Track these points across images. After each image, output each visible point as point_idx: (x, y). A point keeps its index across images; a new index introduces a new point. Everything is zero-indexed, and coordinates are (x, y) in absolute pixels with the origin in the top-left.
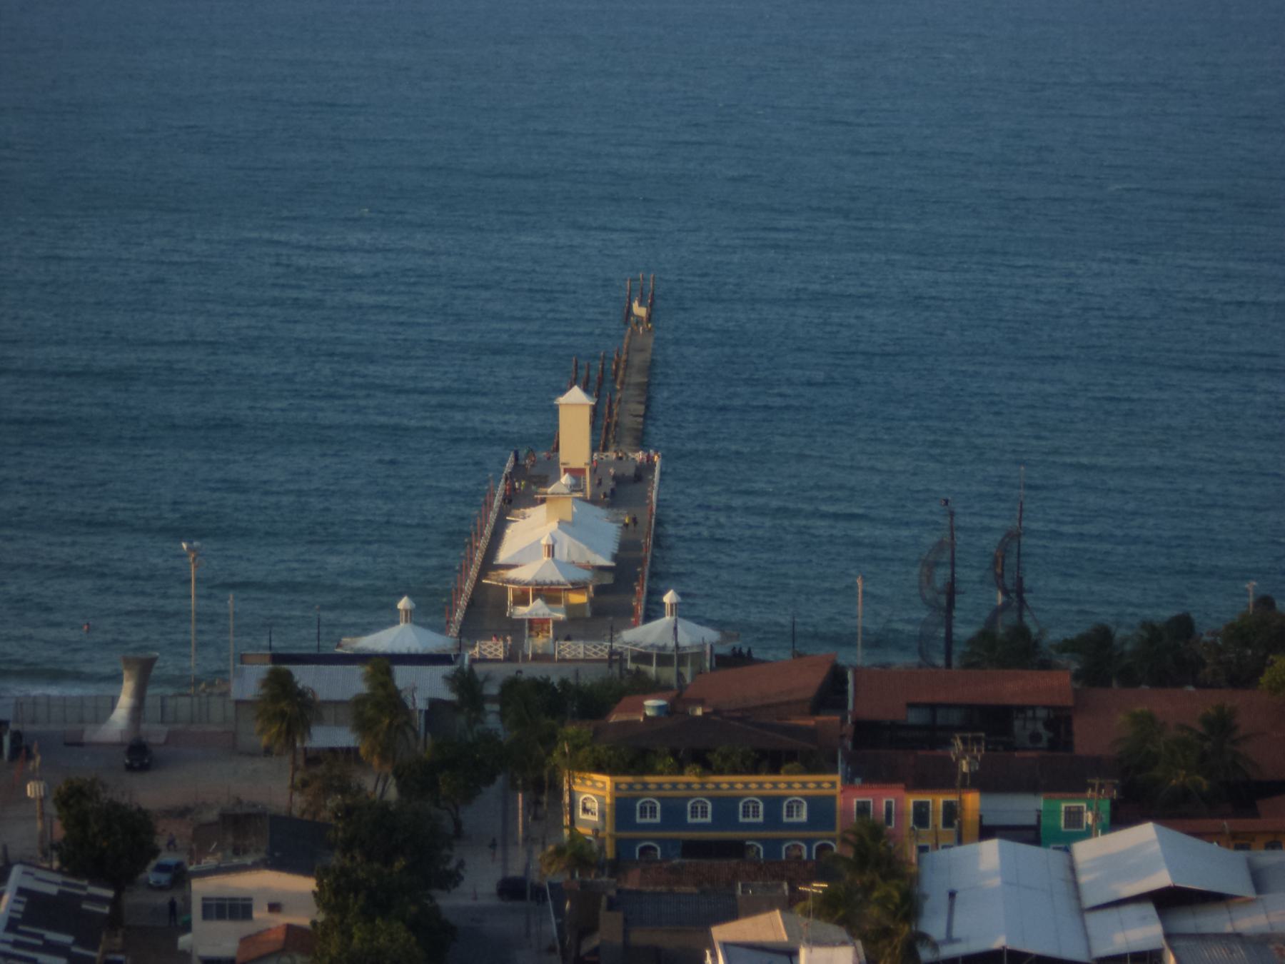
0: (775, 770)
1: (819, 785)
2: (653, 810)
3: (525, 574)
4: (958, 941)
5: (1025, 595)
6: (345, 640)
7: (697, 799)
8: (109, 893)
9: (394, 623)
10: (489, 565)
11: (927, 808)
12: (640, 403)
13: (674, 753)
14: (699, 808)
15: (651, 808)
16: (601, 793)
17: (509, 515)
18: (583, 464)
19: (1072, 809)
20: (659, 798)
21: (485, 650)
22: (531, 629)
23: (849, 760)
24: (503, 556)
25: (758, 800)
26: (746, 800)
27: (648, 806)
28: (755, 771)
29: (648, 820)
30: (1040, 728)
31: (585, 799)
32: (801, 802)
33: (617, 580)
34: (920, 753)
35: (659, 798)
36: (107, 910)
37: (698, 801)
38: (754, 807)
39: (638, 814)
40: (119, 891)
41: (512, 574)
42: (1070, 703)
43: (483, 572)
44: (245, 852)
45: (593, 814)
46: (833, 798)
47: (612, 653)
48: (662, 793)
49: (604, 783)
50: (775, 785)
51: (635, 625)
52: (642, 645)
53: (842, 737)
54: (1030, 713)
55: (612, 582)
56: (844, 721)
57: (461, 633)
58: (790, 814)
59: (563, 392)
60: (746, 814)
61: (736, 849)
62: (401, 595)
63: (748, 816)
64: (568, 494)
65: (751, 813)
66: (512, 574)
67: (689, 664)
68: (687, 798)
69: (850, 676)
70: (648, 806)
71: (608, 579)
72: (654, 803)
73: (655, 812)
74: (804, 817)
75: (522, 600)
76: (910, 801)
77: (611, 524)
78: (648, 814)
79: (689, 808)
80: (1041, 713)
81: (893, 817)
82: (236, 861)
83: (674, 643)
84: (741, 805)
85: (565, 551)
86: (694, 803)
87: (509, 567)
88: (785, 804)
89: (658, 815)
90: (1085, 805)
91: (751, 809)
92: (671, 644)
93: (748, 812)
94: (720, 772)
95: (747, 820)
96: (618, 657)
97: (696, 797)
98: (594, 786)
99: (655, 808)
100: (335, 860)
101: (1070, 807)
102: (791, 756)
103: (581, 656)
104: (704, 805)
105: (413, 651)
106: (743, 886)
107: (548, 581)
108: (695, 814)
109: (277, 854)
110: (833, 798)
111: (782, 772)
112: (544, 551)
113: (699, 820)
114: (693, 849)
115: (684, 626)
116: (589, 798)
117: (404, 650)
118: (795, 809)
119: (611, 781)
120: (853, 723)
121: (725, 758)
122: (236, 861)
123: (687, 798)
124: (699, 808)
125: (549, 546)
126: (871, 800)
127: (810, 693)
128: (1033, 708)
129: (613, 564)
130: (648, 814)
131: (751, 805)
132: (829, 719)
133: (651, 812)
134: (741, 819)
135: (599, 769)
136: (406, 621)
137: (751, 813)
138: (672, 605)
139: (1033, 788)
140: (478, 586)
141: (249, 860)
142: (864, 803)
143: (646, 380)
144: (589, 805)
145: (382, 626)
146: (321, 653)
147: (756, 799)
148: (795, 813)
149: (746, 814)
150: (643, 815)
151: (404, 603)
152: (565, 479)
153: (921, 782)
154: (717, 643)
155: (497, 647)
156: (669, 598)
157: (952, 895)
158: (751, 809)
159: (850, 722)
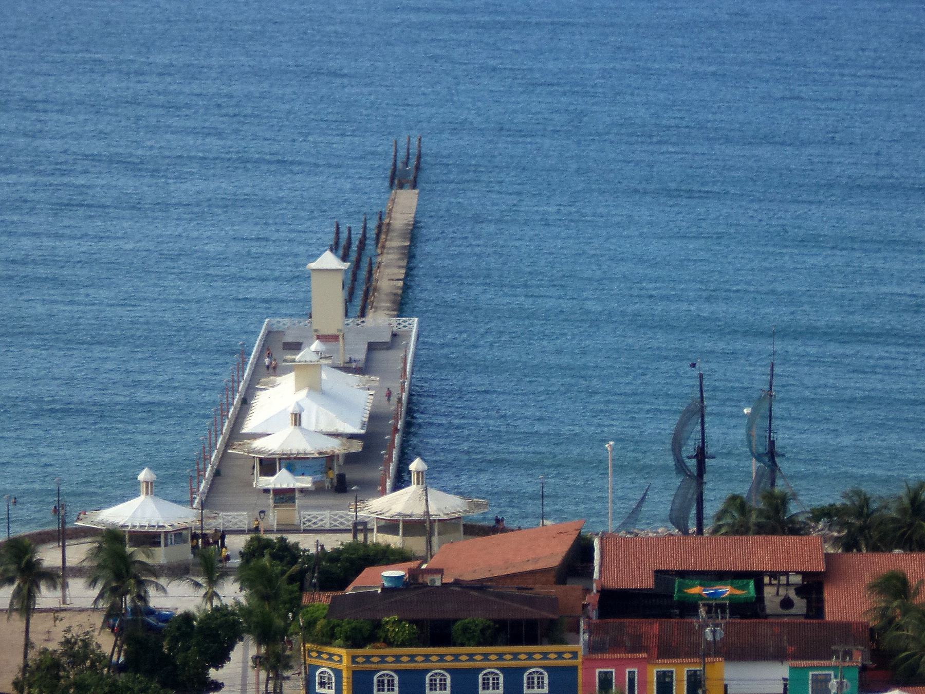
3: (270, 445)
5: (777, 460)
7: (436, 671)
9: (136, 495)
10: (235, 435)
11: (671, 677)
12: (400, 267)
14: (386, 682)
15: (389, 681)
16: (337, 666)
17: (258, 383)
19: (819, 677)
24: (249, 426)
25: (497, 672)
26: (531, 670)
27: (386, 679)
30: (792, 594)
31: (322, 673)
35: (396, 671)
38: (494, 679)
41: (258, 444)
42: (821, 568)
43: (228, 445)
46: (574, 669)
48: (398, 666)
49: (340, 656)
51: (383, 493)
53: (585, 606)
54: (783, 579)
55: (360, 450)
56: (588, 590)
57: (203, 505)
59: (314, 257)
62: (141, 466)
63: (533, 688)
65: (491, 685)
66: (258, 444)
69: (596, 543)
70: (386, 679)
72: (391, 676)
73: (393, 685)
77: (362, 391)
78: (386, 688)
79: (427, 681)
80: (796, 579)
83: (31, 621)
85: (313, 420)
86: (432, 675)
87: (255, 436)
90: (832, 673)
91: (491, 681)
93: (488, 684)
96: (362, 527)
97: (432, 670)
99: (393, 681)
101: (817, 675)
103: (327, 527)
104: (496, 676)
107: (295, 451)
110: (574, 669)
112: (289, 420)
119: (347, 653)
120: (598, 591)
125: (295, 414)
126: (613, 670)
128: (786, 573)
129: (363, 432)
130: (386, 688)
132: (574, 587)
133: (389, 685)
136: (147, 494)
137: (491, 685)
139: (779, 656)
140: (224, 456)
142: (606, 673)
143: (408, 244)
145: (123, 499)
151: (144, 475)
153: (667, 651)
156: (416, 465)
158: (491, 681)
159: (595, 591)
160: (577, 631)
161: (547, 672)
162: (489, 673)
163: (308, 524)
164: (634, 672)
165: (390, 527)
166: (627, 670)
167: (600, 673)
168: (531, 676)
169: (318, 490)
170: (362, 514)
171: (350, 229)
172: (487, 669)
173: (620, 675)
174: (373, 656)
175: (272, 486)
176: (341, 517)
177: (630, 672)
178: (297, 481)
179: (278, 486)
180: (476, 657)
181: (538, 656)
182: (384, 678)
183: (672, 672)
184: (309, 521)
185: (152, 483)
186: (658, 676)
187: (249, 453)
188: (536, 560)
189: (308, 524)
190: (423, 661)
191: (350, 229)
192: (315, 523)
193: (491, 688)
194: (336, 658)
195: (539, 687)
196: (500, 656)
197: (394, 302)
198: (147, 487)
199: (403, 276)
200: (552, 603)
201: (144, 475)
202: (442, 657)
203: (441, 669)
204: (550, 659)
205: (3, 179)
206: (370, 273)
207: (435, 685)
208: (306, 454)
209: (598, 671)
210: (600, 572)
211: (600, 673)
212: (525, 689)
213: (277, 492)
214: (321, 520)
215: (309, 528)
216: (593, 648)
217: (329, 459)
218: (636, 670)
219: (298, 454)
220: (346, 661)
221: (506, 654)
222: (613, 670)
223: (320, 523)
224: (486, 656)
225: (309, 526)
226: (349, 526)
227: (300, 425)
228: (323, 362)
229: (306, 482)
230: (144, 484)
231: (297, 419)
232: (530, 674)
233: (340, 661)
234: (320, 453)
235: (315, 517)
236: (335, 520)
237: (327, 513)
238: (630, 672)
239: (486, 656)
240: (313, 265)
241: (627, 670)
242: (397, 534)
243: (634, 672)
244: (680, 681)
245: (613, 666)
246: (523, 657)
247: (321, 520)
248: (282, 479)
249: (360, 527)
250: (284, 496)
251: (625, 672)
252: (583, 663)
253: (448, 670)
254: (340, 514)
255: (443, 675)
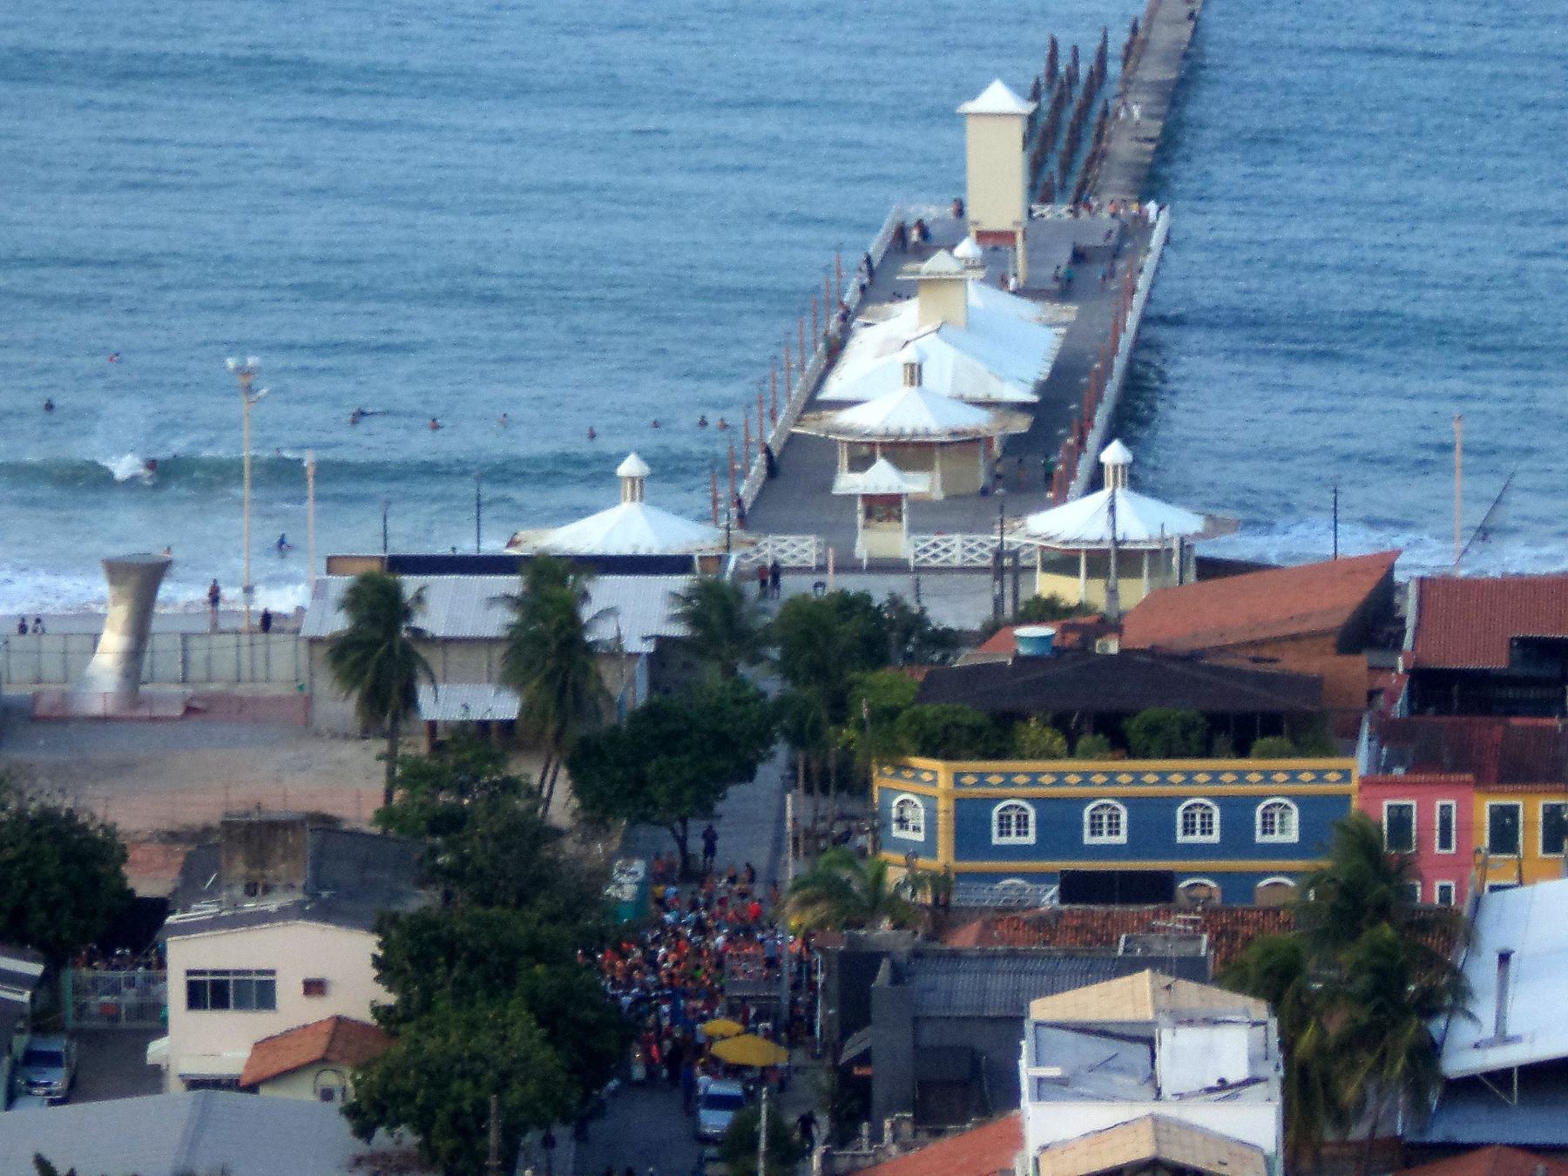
0: (1242, 749)
1: (1320, 775)
2: (1023, 822)
3: (867, 419)
4: (1515, 1039)
6: (523, 534)
8: (36, 969)
13: (1060, 722)
14: (1014, 819)
15: (1018, 817)
16: (930, 791)
18: (1011, 222)
20: (1033, 800)
21: (782, 551)
22: (869, 514)
23: (1387, 732)
25: (1208, 803)
26: (1270, 801)
27: (1014, 814)
28: (1207, 752)
29: (1013, 839)
31: (902, 802)
32: (1286, 807)
33: (1035, 426)
34: (1516, 722)
35: (1032, 800)
36: (26, 997)
37: (1102, 806)
38: (1203, 816)
39: (995, 829)
40: (56, 958)
41: (845, 418)
44: (267, 890)
45: (916, 829)
46: (1347, 798)
47: (999, 554)
49: (934, 773)
50: (982, 778)
52: (1059, 540)
58: (1268, 828)
59: (974, 93)
60: (1189, 829)
61: (1158, 888)
64: (958, 273)
65: (1198, 826)
66: (845, 418)
67: (1145, 571)
68: (1084, 801)
70: (1014, 814)
71: (1021, 424)
72: (1023, 809)
73: (1026, 825)
74: (1293, 836)
75: (861, 463)
76: (1484, 806)
81: (1454, 833)
82: (250, 906)
84: (1180, 811)
88: (1180, 811)
89: (1032, 829)
91: (1198, 820)
92: (1108, 537)
93: (1193, 824)
94: (1145, 755)
95: (1190, 839)
98: (916, 779)
99: (1026, 817)
100: (421, 901)
102: (1272, 724)
103: (957, 562)
104: (1207, 812)
105: (642, 552)
106: (1128, 941)
108: (1114, 829)
109: (325, 894)
110: (1347, 798)
111: (1254, 750)
113: (1105, 839)
114: (1076, 887)
115: (1127, 503)
116: (908, 801)
117: (627, 551)
118: (1277, 819)
119: (947, 769)
120: (1407, 671)
121: (1153, 729)
122: (250, 906)
123: (1084, 801)
124: (1014, 819)
125: (912, 365)
126: (1414, 803)
127: (1338, 619)
129: (1035, 399)
131: (1198, 812)
133: (1019, 825)
134: (1181, 838)
135: (931, 749)
137: (1198, 826)
138: (1115, 467)
141: (272, 905)
142: (1401, 808)
144: (908, 813)
146: (459, 552)
147: (1208, 803)
148: (1277, 827)
149: (1189, 829)
150: (1004, 830)
152: (967, 248)
154: (1197, 535)
155: (804, 546)
157: (1504, 958)
158: (1198, 820)
160: (1355, 736)
161: (1035, 806)
162: (1195, 805)
163: (923, 556)
164: (1450, 807)
165: (1063, 562)
166: (1439, 803)
167: (1390, 807)
168: (1004, 813)
169: (954, 499)
170: (1013, 539)
171: (1075, 50)
172: (1191, 797)
173: (1426, 809)
174: (991, 774)
175: (860, 491)
176: (981, 545)
177: (1442, 807)
178: (905, 480)
179: (871, 491)
180: (1249, 777)
181: (1280, 777)
182: (1101, 812)
183: (1517, 807)
184: (925, 551)
185: (641, 481)
186: (1545, 814)
187: (828, 432)
188: (1305, 617)
189: (923, 556)
190: (1053, 784)
191: (1075, 50)
192: (935, 556)
193: (1198, 832)
194: (927, 777)
195: (1203, 832)
196: (1215, 776)
197: (1136, 179)
198: (633, 487)
199: (1155, 133)
200: (1313, 685)
201: (631, 466)
202: (1112, 777)
203: (1278, 796)
204: (1042, 785)
205: (1554, 36)
206: (1101, 127)
207: (1101, 825)
208: (928, 434)
209: (1386, 803)
210: (1415, 638)
211: (1390, 807)
212: (1258, 833)
213: (869, 499)
214: (946, 551)
215: (924, 565)
216: (1380, 767)
217: (965, 444)
218: (1452, 803)
219: (915, 434)
220: (944, 781)
221: (1071, 773)
222: (1414, 803)
223: (944, 556)
224: (1189, 777)
225: (924, 560)
226: (982, 556)
227: (920, 383)
228: (970, 274)
229: (918, 484)
230: (629, 485)
231: (914, 374)
232: (1188, 808)
233: (934, 782)
234: (954, 434)
235: (935, 545)
236: (971, 551)
237: (957, 539)
238: (1442, 807)
239: (1189, 777)
240: (969, 107)
241: (1439, 803)
242: (1076, 574)
243: (1450, 807)
244: (1530, 824)
245: (1411, 796)
246: (1176, 778)
247: (946, 551)
248: (882, 477)
249: (1006, 567)
250: (883, 507)
251: (1433, 806)
252: (1360, 789)
253: (1125, 800)
254: (979, 541)
255: (1114, 809)
